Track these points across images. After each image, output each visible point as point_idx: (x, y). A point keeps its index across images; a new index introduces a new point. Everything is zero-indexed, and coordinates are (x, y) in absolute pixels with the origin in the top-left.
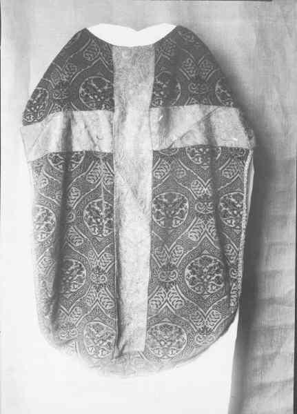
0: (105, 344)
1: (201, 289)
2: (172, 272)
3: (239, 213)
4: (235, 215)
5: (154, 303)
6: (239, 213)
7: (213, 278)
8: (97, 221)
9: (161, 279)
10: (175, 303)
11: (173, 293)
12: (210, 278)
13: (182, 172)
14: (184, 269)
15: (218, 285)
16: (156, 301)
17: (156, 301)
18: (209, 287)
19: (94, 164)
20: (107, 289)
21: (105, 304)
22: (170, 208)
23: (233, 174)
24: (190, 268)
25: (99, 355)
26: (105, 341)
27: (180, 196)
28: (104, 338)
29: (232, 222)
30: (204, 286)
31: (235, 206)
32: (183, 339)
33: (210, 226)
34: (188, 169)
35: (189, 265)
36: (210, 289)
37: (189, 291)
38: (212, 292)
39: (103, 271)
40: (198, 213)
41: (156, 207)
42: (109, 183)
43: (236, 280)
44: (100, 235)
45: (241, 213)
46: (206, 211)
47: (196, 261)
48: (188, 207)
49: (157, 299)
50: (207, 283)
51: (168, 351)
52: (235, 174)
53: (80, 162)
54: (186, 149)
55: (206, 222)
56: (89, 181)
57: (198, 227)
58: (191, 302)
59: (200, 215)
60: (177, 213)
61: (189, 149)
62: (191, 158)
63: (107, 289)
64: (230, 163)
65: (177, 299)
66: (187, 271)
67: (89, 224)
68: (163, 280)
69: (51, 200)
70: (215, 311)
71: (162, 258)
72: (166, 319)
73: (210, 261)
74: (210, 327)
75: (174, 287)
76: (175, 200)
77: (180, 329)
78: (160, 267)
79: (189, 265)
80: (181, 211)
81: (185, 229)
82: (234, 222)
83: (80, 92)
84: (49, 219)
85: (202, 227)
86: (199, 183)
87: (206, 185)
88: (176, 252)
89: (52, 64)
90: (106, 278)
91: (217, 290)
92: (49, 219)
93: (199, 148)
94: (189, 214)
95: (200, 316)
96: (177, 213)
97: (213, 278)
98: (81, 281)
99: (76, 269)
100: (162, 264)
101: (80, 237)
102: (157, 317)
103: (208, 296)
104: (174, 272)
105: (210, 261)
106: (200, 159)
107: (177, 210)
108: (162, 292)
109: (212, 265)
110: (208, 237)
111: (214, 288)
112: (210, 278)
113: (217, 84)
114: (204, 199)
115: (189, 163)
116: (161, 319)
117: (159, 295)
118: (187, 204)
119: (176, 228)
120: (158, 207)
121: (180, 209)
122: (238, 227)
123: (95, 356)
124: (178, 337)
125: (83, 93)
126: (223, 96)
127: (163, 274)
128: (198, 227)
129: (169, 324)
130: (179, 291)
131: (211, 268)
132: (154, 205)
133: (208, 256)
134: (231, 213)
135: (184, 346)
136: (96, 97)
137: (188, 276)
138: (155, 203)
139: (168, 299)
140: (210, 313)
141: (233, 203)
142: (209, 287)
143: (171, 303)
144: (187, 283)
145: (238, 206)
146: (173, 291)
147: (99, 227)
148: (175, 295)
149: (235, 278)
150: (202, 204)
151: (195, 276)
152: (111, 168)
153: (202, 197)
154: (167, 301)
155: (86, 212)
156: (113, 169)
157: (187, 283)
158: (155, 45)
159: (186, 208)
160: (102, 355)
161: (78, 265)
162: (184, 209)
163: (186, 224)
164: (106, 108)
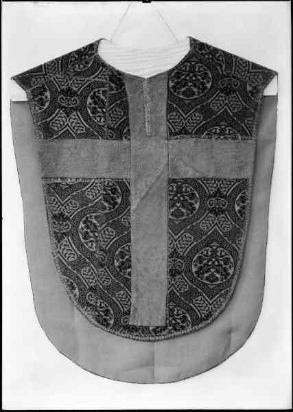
8: (218, 262)
12: (208, 262)
16: (256, 80)
17: (256, 80)
18: (210, 253)
19: (227, 192)
20: (200, 316)
23: (104, 232)
26: (205, 265)
31: (96, 228)
39: (211, 212)
40: (88, 303)
46: (69, 105)
48: (193, 266)
49: (254, 81)
51: (212, 255)
63: (200, 316)
67: (93, 113)
79: (194, 212)
80: (123, 257)
92: (241, 207)
96: (206, 261)
100: (223, 215)
101: (197, 305)
107: (202, 54)
109: (206, 275)
112: (208, 262)
121: (179, 80)
127: (223, 206)
129: (185, 98)
147: (181, 192)
153: (231, 93)
159: (196, 265)
161: (200, 276)
162: (199, 265)
163: (196, 250)
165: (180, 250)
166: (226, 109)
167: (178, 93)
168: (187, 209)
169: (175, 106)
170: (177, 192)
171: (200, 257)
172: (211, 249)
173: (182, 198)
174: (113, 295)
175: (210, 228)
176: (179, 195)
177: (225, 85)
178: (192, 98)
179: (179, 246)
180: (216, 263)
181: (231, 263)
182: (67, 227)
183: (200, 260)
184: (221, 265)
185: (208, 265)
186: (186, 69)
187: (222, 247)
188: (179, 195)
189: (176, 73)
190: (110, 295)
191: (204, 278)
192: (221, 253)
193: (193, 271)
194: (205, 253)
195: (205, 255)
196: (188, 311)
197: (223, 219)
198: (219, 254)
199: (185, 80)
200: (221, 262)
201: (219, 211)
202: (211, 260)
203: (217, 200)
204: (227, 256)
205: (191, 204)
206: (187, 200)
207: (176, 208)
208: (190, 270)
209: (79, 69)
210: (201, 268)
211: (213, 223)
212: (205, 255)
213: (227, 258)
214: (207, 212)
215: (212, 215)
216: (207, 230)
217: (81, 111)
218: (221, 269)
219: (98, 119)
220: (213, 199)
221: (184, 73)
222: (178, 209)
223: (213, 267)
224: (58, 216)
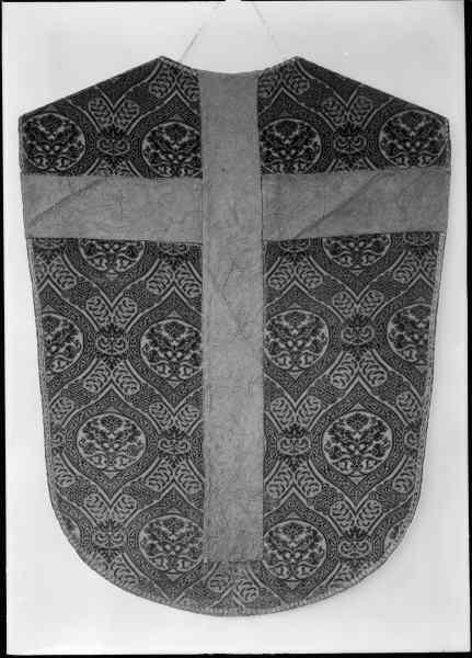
0: (186, 551)
1: (348, 467)
2: (300, 441)
3: (421, 337)
4: (416, 342)
5: (274, 489)
6: (421, 337)
7: (371, 448)
14: (321, 434)
16: (156, 282)
17: (277, 486)
19: (99, 162)
21: (187, 485)
25: (179, 569)
26: (189, 155)
27: (311, 317)
28: (184, 541)
30: (354, 463)
34: (325, 273)
37: (329, 470)
39: (184, 434)
41: (389, 137)
42: (193, 295)
43: (414, 450)
44: (174, 378)
45: (426, 337)
48: (390, 439)
52: (414, 275)
53: (137, 259)
54: (324, 240)
55: (358, 359)
56: (151, 290)
57: (345, 366)
59: (346, 347)
61: (329, 242)
64: (406, 258)
65: (127, 380)
66: (327, 437)
69: (77, 311)
72: (176, 117)
74: (362, 528)
78: (406, 425)
83: (144, 147)
84: (72, 339)
86: (349, 296)
89: (92, 87)
90: (373, 331)
93: (349, 242)
96: (308, 345)
98: (135, 452)
99: (126, 432)
100: (410, 421)
103: (361, 271)
104: (304, 441)
110: (362, 382)
111: (371, 463)
112: (303, 345)
114: (107, 527)
115: (328, 265)
116: (284, 514)
120: (275, 335)
122: (421, 362)
123: (173, 571)
124: (312, 546)
125: (148, 149)
126: (392, 150)
128: (345, 366)
130: (314, 468)
132: (268, 333)
133: (362, 413)
136: (171, 156)
138: (270, 328)
141: (42, 133)
145: (421, 325)
149: (414, 447)
152: (195, 272)
155: (145, 341)
156: (201, 275)
157: (327, 455)
158: (264, 78)
160: (184, 567)
162: (318, 338)
164: (186, 174)
166: (295, 401)
167: (373, 419)
169: (303, 104)
171: (318, 351)
174: (143, 388)
176: (357, 249)
182: (122, 346)
183: (317, 347)
186: (306, 358)
189: (382, 455)
190: (331, 486)
191: (189, 133)
196: (395, 357)
199: (366, 443)
209: (185, 374)
213: (274, 354)
214: (128, 133)
215: (121, 127)
219: (161, 369)
221: (370, 455)
222: (421, 318)
223: (357, 440)
224: (107, 329)
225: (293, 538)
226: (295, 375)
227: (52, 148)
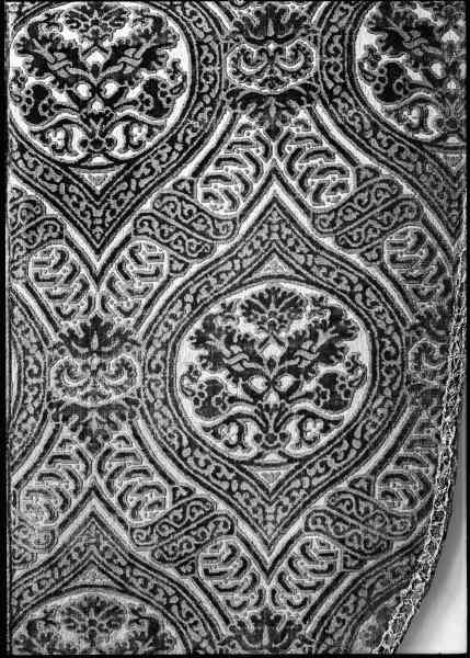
1: (248, 439)
2: (112, 363)
7: (309, 386)
9: (58, 394)
10: (131, 500)
11: (122, 455)
13: (151, 497)
14: (171, 348)
15: (332, 416)
18: (291, 428)
22: (95, 70)
24: (200, 341)
29: (424, 116)
32: (175, 70)
33: (290, 148)
35: (198, 325)
36: (295, 435)
37: (192, 444)
38: (305, 450)
47: (229, 308)
50: (280, 410)
58: (200, 492)
60: (133, 94)
62: (197, 422)
66: (188, 354)
68: (70, 399)
70: (314, 538)
71: (61, 297)
73: (114, 616)
74: (286, 612)
75: (126, 430)
76: (124, 33)
77: (158, 22)
79: (198, 325)
81: (181, 164)
82: (433, 113)
85: (257, 151)
87: (276, 187)
88: (131, 268)
91: (324, 440)
94: (197, 95)
95: (245, 564)
96: (133, 94)
97: (133, 93)
102: (50, 564)
105: (296, 305)
106: (252, 429)
108: (70, 450)
111: (313, 428)
113: (363, 30)
117: (60, 467)
118: (180, 53)
119: (129, 162)
127: (68, 367)
131: (298, 339)
134: (416, 77)
135: (181, 102)
137: (192, 373)
139: (102, 483)
140: (295, 550)
141: (426, 30)
142: (291, 428)
143: (114, 501)
144: (188, 405)
146: (119, 447)
148: (130, 464)
150: (254, 50)
151: (221, 376)
154: (95, 490)
162: (162, 74)
163: (185, 145)
165: (250, 135)
168: (54, 44)
170: (283, 416)
171: (337, 405)
172: (289, 449)
173: (258, 383)
175: (125, 253)
177: (112, 363)
178: (76, 597)
179: (257, 151)
180: (258, 383)
181: (185, 391)
184: (61, 83)
185: (294, 371)
187: (65, 166)
188: (273, 399)
192: (241, 433)
193: (182, 46)
194: (313, 428)
195: (314, 417)
197: (67, 307)
198: (252, 429)
200: (61, 97)
201: (86, 342)
202: (108, 102)
203: (96, 395)
204: (209, 423)
205: (215, 360)
206: (234, 376)
207: (106, 44)
208: (195, 47)
210: (150, 59)
211: (280, 579)
212: (314, 417)
216: (136, 241)
217: (329, 100)
218: (59, 63)
220: (115, 398)
223: (271, 363)
225: (97, 41)
226: (96, 180)
227: (96, 90)
